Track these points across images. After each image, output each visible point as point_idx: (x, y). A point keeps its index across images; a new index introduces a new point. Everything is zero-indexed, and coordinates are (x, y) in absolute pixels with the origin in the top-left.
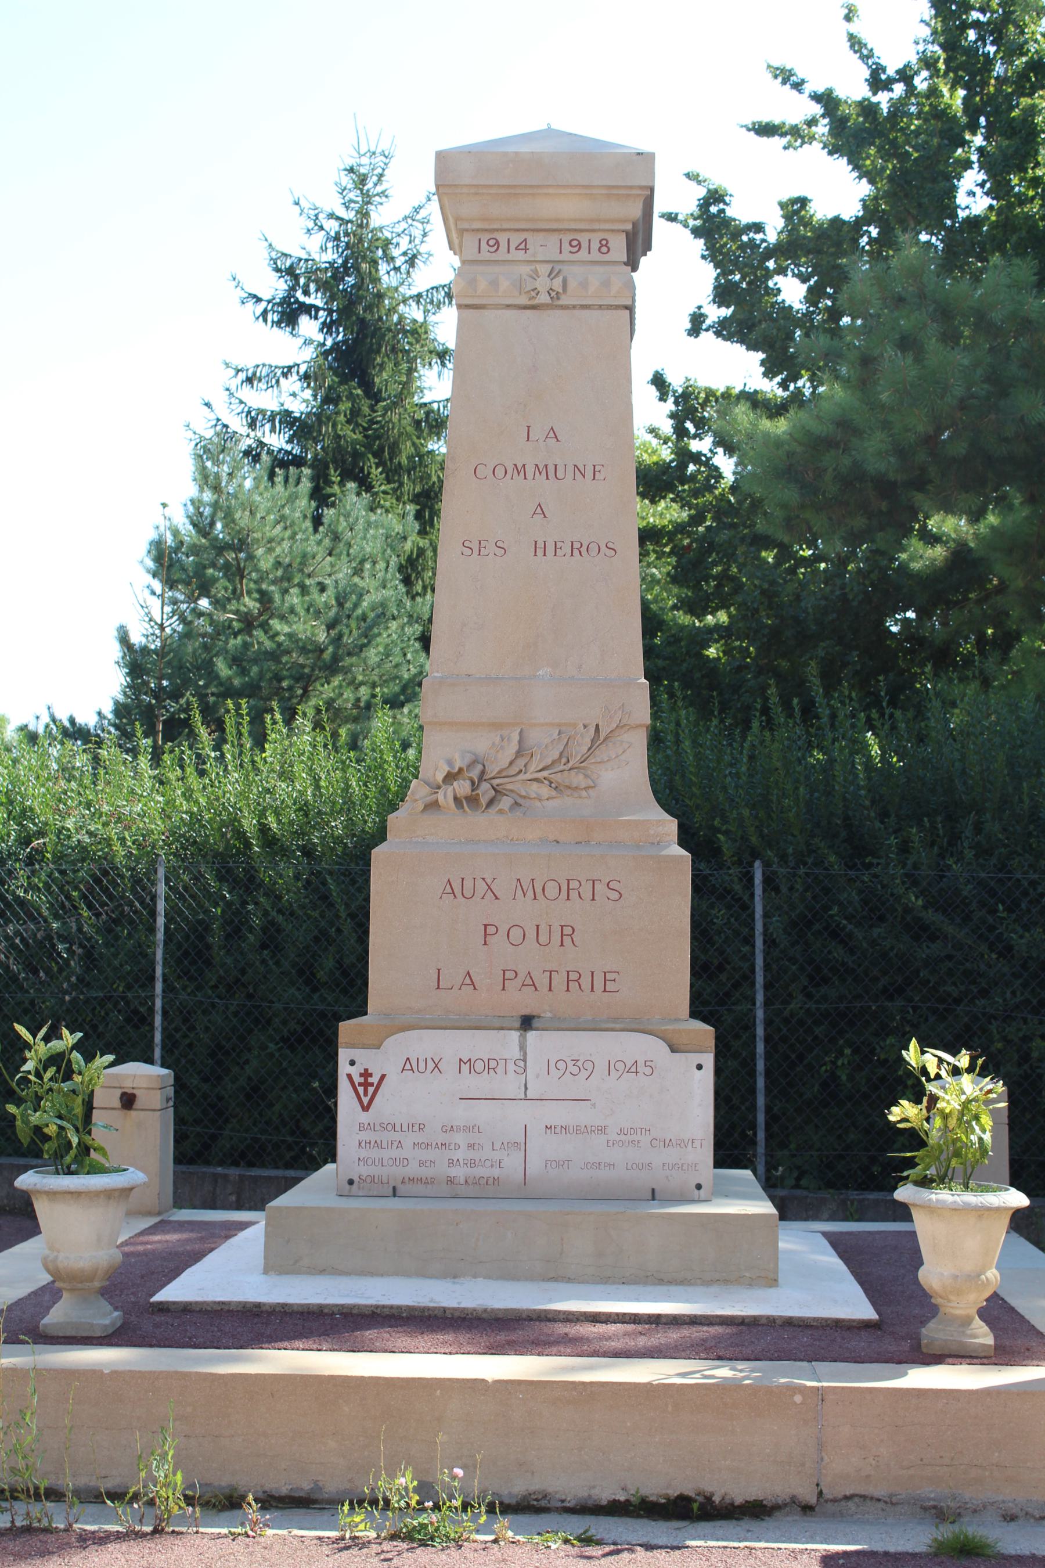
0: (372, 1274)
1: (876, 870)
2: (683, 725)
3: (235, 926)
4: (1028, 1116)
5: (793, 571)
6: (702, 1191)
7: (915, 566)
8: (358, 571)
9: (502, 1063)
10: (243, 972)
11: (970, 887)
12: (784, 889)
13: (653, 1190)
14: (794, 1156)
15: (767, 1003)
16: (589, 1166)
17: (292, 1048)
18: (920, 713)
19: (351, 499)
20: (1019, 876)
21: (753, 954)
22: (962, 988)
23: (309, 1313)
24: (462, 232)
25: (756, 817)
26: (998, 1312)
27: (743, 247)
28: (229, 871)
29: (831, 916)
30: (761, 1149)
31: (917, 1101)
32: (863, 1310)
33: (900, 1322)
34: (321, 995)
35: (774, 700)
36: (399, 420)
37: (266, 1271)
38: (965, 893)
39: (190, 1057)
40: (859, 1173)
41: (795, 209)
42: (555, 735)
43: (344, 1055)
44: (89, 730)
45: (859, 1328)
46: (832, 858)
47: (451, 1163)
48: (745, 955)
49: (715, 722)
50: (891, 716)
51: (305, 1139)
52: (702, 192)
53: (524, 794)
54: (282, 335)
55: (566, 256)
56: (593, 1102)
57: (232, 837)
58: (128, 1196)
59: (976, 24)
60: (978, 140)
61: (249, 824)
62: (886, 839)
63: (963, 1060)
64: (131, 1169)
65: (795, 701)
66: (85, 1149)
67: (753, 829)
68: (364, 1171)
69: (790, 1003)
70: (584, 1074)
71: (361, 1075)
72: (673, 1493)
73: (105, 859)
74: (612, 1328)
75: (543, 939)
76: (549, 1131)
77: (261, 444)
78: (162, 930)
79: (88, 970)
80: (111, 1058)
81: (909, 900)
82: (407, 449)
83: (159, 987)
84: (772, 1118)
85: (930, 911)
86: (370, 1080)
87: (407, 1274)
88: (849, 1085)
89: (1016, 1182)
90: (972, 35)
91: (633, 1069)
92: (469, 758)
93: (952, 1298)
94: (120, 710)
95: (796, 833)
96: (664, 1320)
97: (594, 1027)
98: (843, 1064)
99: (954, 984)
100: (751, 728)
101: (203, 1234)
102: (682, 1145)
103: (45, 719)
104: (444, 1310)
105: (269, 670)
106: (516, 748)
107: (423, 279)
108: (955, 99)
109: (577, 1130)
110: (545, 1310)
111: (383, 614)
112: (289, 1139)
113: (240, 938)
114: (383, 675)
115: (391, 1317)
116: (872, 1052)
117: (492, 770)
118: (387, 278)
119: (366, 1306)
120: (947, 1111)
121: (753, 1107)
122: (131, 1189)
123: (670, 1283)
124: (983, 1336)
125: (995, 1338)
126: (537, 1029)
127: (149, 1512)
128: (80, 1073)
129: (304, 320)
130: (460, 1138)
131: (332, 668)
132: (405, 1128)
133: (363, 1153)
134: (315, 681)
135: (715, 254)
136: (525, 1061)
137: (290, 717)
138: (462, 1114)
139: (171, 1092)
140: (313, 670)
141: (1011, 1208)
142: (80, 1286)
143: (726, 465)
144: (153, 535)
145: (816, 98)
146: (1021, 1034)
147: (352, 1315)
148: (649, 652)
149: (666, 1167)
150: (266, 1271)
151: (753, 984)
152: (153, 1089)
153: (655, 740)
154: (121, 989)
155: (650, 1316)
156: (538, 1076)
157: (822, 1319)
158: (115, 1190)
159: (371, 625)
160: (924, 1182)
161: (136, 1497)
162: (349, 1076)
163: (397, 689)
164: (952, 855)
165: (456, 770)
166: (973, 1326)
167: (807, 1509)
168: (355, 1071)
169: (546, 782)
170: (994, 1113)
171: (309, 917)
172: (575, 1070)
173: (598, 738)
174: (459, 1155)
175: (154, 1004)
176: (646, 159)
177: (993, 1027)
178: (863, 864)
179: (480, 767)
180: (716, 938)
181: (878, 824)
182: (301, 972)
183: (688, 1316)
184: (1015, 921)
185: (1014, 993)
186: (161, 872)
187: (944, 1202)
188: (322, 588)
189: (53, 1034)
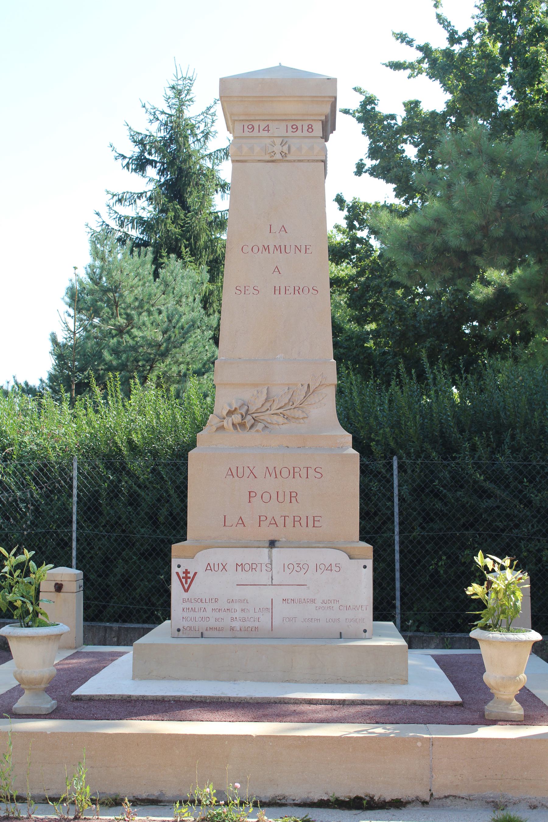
0: (190, 679)
1: (459, 461)
3: (114, 492)
5: (412, 300)
7: (478, 297)
8: (179, 302)
11: (509, 469)
12: (409, 471)
13: (341, 633)
14: (416, 614)
15: (401, 532)
16: (306, 620)
17: (146, 559)
18: (480, 377)
19: (173, 263)
21: (393, 506)
22: (505, 523)
23: (157, 700)
24: (234, 121)
26: (526, 697)
27: (384, 127)
28: (112, 464)
30: (398, 611)
31: (482, 584)
32: (454, 696)
33: (473, 703)
36: (200, 223)
37: (133, 678)
40: (451, 623)
41: (412, 107)
42: (286, 390)
43: (174, 562)
44: (35, 389)
47: (232, 619)
48: (389, 506)
52: (362, 98)
53: (269, 421)
54: (136, 177)
55: (290, 134)
58: (59, 639)
59: (507, 7)
60: (509, 70)
61: (120, 439)
63: (507, 562)
64: (61, 624)
65: (413, 371)
68: (186, 624)
69: (413, 533)
70: (303, 571)
71: (184, 573)
72: (353, 795)
73: (45, 458)
74: (319, 707)
75: (281, 499)
76: (284, 602)
77: (126, 235)
79: (36, 517)
82: (203, 238)
85: (487, 483)
86: (189, 575)
87: (209, 679)
88: (445, 576)
90: (504, 13)
91: (329, 568)
93: (501, 689)
94: (52, 378)
96: (347, 703)
98: (442, 565)
99: (501, 521)
102: (356, 609)
103: (12, 383)
107: (213, 145)
108: (495, 48)
109: (300, 601)
111: (193, 325)
112: (145, 607)
115: (201, 702)
117: (253, 409)
118: (194, 146)
119: (188, 696)
121: (394, 588)
122: (61, 635)
123: (350, 682)
124: (517, 709)
125: (525, 710)
127: (72, 808)
128: (34, 573)
129: (149, 168)
130: (237, 606)
131: (164, 355)
133: (185, 615)
135: (369, 131)
140: (155, 356)
141: (532, 641)
142: (34, 687)
143: (375, 243)
144: (69, 284)
145: (420, 48)
146: (537, 548)
148: (336, 345)
149: (347, 621)
150: (133, 678)
151: (393, 522)
153: (340, 392)
154: (54, 528)
155: (339, 700)
156: (278, 573)
157: (432, 701)
159: (185, 333)
160: (486, 628)
161: (65, 800)
162: (177, 573)
164: (499, 452)
166: (512, 704)
167: (425, 803)
168: (180, 571)
169: (282, 415)
170: (523, 590)
172: (298, 569)
173: (309, 391)
174: (236, 615)
175: (72, 535)
176: (332, 82)
177: (522, 544)
178: (452, 457)
179: (246, 407)
181: (458, 436)
182: (151, 518)
183: (360, 700)
184: (532, 488)
185: (533, 526)
187: (496, 638)
188: (160, 312)
189: (19, 552)
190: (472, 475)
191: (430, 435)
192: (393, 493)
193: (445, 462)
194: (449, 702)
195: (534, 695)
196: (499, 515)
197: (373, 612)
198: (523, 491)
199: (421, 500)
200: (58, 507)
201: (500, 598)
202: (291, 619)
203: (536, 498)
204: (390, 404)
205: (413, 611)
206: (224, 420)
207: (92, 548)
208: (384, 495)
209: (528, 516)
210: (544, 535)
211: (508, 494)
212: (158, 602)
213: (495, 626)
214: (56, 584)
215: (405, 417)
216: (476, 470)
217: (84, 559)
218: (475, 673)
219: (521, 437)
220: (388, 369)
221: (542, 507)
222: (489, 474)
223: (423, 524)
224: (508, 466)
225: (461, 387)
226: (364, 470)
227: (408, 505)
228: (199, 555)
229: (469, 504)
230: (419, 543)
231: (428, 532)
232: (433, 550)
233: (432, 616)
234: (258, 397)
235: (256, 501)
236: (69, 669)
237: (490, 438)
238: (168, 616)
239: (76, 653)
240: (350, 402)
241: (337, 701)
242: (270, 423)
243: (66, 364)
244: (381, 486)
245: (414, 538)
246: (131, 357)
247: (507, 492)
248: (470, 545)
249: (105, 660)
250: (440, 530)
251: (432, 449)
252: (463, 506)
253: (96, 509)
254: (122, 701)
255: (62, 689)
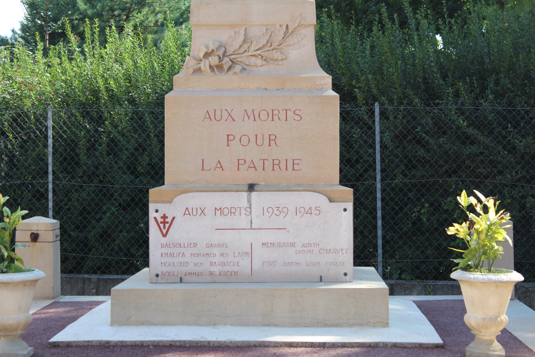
0: (169, 324)
1: (442, 107)
2: (335, 29)
4: (525, 239)
6: (347, 277)
9: (238, 209)
10: (97, 168)
11: (493, 115)
12: (391, 118)
13: (321, 277)
14: (398, 262)
15: (383, 180)
16: (286, 264)
17: (124, 209)
20: (519, 108)
21: (375, 153)
22: (489, 170)
23: (135, 346)
25: (376, 79)
28: (88, 113)
29: (417, 132)
30: (380, 259)
34: (140, 179)
35: (385, 15)
37: (112, 324)
38: (490, 118)
39: (68, 216)
40: (434, 271)
42: (264, 31)
43: (152, 207)
44: (7, 40)
45: (432, 348)
46: (417, 100)
47: (211, 264)
48: (370, 154)
49: (353, 27)
50: (450, 22)
51: (132, 255)
53: (248, 63)
56: (287, 230)
57: (89, 94)
58: (35, 285)
62: (446, 90)
64: (37, 270)
65: (395, 15)
66: (12, 260)
67: (374, 85)
68: (164, 269)
69: (395, 180)
70: (283, 215)
71: (162, 217)
73: (19, 108)
74: (300, 350)
75: (259, 142)
76: (264, 246)
78: (51, 146)
79: (11, 169)
80: (25, 212)
81: (459, 122)
83: (50, 177)
84: (386, 242)
85: (471, 128)
86: (167, 220)
87: (189, 324)
88: (428, 224)
89: (518, 269)
91: (309, 212)
92: (217, 44)
93: (482, 330)
94: (24, 28)
95: (397, 87)
96: (327, 345)
97: (288, 190)
98: (424, 212)
99: (484, 168)
100: (372, 31)
101: (78, 307)
102: (336, 252)
104: (209, 342)
105: (107, 5)
106: (243, 38)
109: (280, 245)
110: (263, 341)
112: (124, 258)
113: (94, 150)
114: (171, 7)
115: (181, 346)
116: (440, 205)
117: (230, 50)
119: (167, 341)
120: (480, 230)
121: (376, 237)
122: (37, 280)
123: (330, 326)
125: (506, 352)
126: (257, 191)
128: (8, 217)
130: (216, 251)
132: (186, 246)
133: (164, 260)
134: (133, 11)
136: (250, 208)
137: (121, 29)
138: (217, 237)
139: (58, 232)
140: (131, 5)
141: (514, 282)
142: (10, 334)
146: (520, 194)
147: (159, 346)
149: (328, 264)
150: (112, 324)
151: (375, 170)
152: (48, 230)
153: (320, 40)
154: (30, 179)
155: (320, 343)
156: (257, 216)
157: (413, 343)
158: (28, 281)
160: (467, 268)
162: (155, 218)
163: (178, 15)
164: (483, 98)
165: (210, 51)
166: (493, 345)
168: (158, 216)
169: (260, 57)
171: (133, 137)
172: (278, 213)
173: (288, 32)
174: (216, 260)
175: (48, 187)
177: (506, 191)
178: (434, 103)
179: (223, 49)
180: (354, 145)
181: (442, 82)
182: (129, 168)
183: (341, 343)
184: (517, 133)
185: (517, 172)
186: (50, 114)
187: (478, 278)
190: (455, 121)
191: (412, 81)
192: (374, 140)
193: (428, 108)
194: (430, 344)
195: (516, 338)
196: (482, 162)
197: (354, 259)
198: (507, 137)
199: (404, 147)
200: (34, 158)
201: (482, 239)
202: (271, 263)
203: (520, 144)
204: (372, 50)
205: (396, 259)
206: (201, 62)
207: (70, 200)
208: (366, 142)
209: (512, 162)
210: (528, 182)
211: (491, 140)
212: (137, 253)
213: (477, 267)
214: (32, 234)
215: (388, 63)
216: (459, 116)
217: (61, 211)
218: (457, 317)
219: (505, 81)
220: (370, 17)
221: (526, 153)
222: (473, 121)
223: (406, 171)
224: (492, 112)
225: (444, 32)
226: (344, 116)
227: (390, 152)
228: (177, 199)
229: (452, 151)
230: (401, 190)
231: (410, 179)
232: (415, 197)
233: (414, 264)
234: (235, 38)
235: (235, 144)
236: (46, 319)
237: (474, 83)
238: (147, 265)
239: (54, 303)
240: (330, 48)
241: (318, 344)
242: (248, 65)
243: (38, 13)
244: (363, 133)
245: (396, 185)
246: (106, 6)
247: (491, 138)
248: (453, 192)
249: (83, 309)
250: (423, 177)
251: (414, 95)
252: (446, 153)
253: (73, 159)
254: (100, 346)
255: (39, 337)
